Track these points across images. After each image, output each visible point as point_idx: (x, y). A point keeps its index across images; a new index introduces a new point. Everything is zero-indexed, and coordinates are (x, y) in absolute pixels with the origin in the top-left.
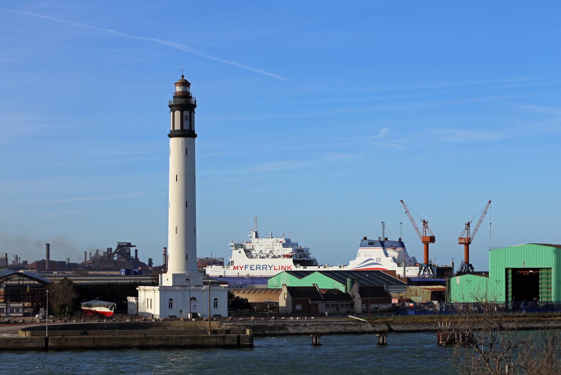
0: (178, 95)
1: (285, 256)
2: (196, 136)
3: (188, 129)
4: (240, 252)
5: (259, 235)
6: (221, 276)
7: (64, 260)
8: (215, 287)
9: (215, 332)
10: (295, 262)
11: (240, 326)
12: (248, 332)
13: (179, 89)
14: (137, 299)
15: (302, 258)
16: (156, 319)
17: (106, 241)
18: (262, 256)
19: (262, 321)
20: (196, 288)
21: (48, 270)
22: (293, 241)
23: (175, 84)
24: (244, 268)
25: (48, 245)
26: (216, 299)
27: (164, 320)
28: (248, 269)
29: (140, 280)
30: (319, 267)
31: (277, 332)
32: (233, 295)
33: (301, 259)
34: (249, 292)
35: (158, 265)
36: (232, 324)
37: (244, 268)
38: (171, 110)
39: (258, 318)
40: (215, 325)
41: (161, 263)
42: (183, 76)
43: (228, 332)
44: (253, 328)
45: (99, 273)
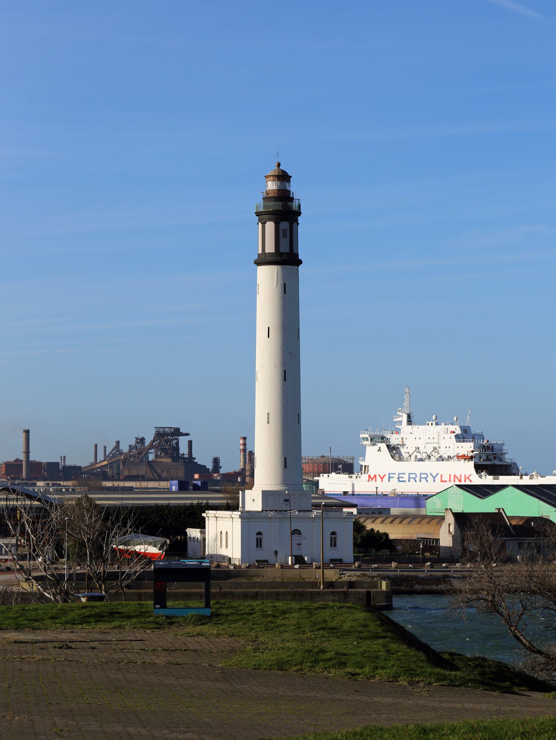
0: (270, 195)
1: (459, 457)
2: (300, 262)
3: (288, 251)
4: (379, 450)
5: (413, 419)
6: (345, 493)
7: (57, 459)
8: (332, 513)
9: (330, 585)
10: (479, 468)
11: (373, 577)
12: (384, 586)
13: (272, 186)
14: (203, 533)
15: (491, 461)
16: (235, 566)
17: (132, 426)
18: (419, 456)
19: (409, 570)
20: (302, 514)
21: (27, 479)
22: (475, 430)
23: (267, 177)
24: (386, 478)
25: (27, 432)
26: (333, 533)
27: (249, 567)
28: (394, 480)
29: (207, 499)
30: (521, 478)
31: (434, 587)
32: (364, 527)
33: (488, 463)
34: (391, 522)
35: (231, 471)
36: (359, 573)
37: (386, 478)
38: (259, 220)
39: (404, 565)
40: (331, 575)
41: (242, 473)
42: (279, 165)
43: (351, 585)
44: (393, 581)
45: (121, 484)
